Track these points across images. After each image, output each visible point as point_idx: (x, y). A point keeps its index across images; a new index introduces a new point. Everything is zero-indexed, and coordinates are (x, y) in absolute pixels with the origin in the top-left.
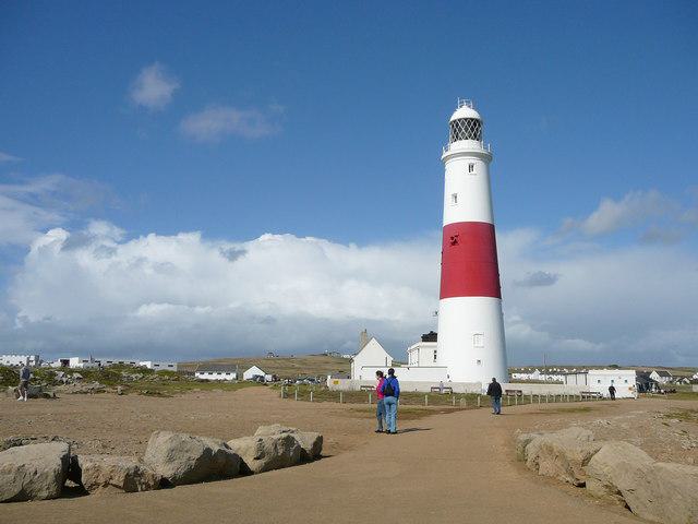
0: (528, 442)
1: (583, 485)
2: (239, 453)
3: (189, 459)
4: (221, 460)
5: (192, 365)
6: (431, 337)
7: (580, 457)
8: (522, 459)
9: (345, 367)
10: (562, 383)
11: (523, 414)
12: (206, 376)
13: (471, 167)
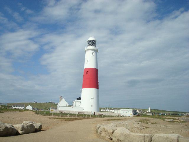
0: (99, 127)
1: (112, 139)
2: (17, 129)
4: (11, 130)
5: (12, 104)
6: (79, 99)
7: (111, 131)
8: (97, 132)
9: (55, 106)
10: (113, 112)
11: (106, 120)
12: (15, 107)
13: (92, 53)
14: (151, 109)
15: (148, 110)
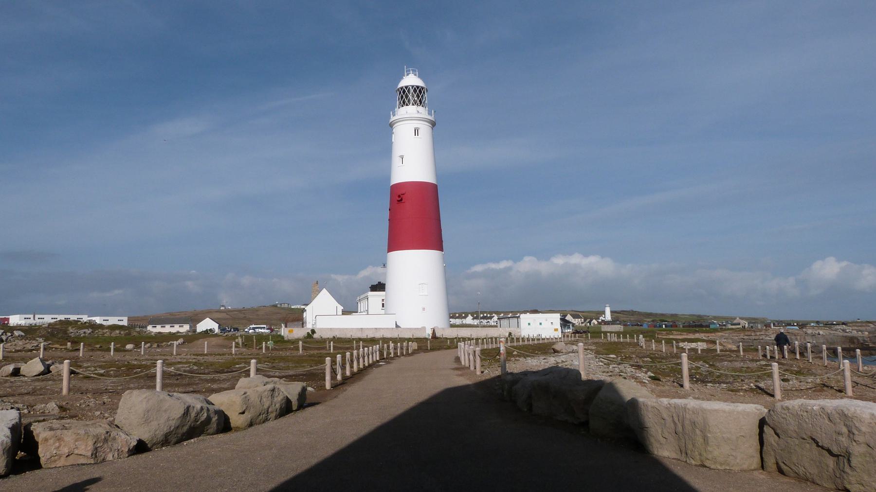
3: (168, 419)
6: (379, 287)
12: (159, 329)
13: (416, 131)
14: (612, 312)
15: (604, 313)
